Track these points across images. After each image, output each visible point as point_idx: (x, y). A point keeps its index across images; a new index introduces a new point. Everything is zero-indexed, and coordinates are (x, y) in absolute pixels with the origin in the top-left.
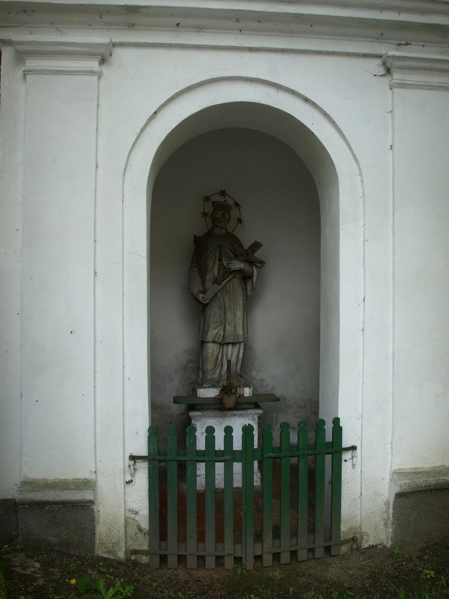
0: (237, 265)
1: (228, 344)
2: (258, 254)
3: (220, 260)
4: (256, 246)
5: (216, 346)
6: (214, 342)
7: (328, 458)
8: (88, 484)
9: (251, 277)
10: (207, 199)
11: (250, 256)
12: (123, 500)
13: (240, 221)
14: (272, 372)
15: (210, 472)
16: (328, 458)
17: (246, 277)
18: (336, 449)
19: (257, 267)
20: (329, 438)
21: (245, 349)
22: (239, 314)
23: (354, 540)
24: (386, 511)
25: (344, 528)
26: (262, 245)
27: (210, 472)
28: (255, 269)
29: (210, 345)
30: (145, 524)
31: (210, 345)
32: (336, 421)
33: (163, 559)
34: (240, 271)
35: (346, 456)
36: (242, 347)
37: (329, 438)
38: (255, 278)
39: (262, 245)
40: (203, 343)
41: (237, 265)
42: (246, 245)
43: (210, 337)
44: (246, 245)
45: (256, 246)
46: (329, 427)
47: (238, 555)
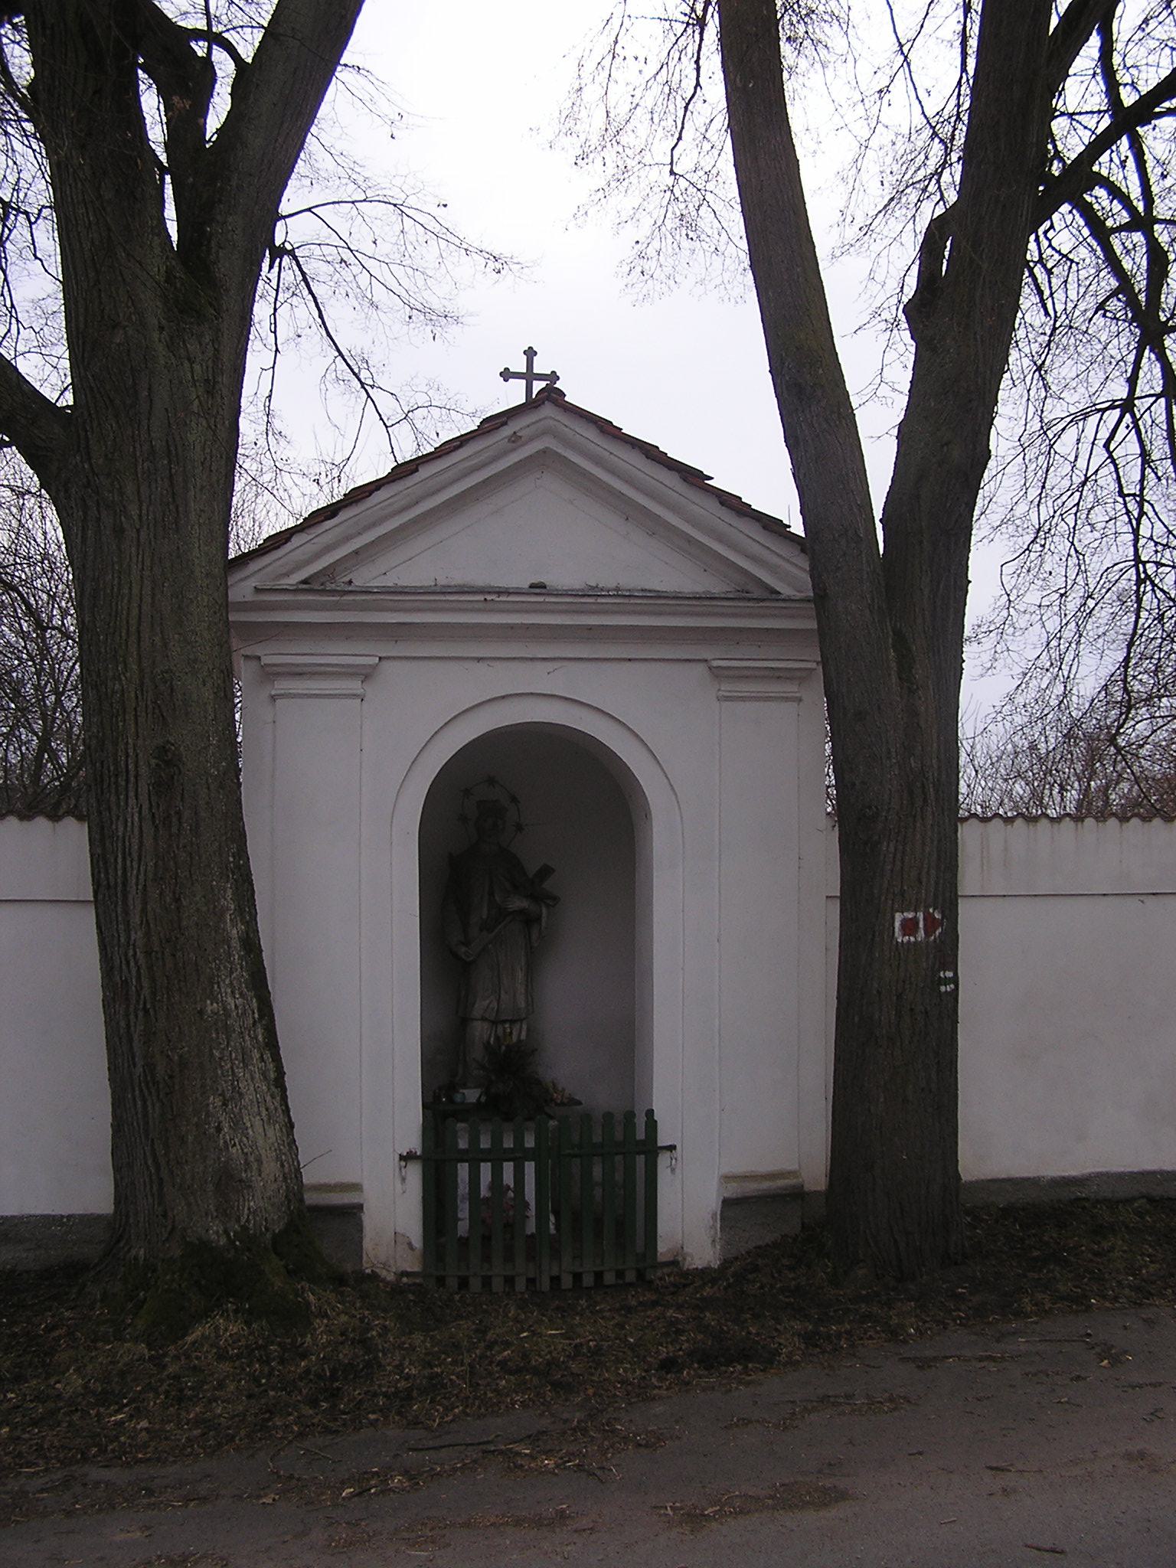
0: (518, 903)
1: (504, 1021)
2: (547, 885)
3: (491, 894)
4: (546, 872)
5: (486, 1025)
6: (483, 1019)
7: (641, 1160)
8: (356, 1187)
9: (539, 919)
10: (467, 792)
11: (538, 889)
12: (393, 1216)
13: (519, 828)
14: (568, 1065)
15: (497, 1174)
16: (641, 1160)
17: (529, 920)
18: (651, 1149)
19: (548, 906)
20: (641, 1135)
21: (528, 1030)
22: (520, 975)
23: (674, 1263)
24: (713, 1227)
25: (662, 1247)
26: (554, 870)
27: (497, 1174)
28: (544, 910)
29: (478, 1025)
30: (417, 1242)
31: (478, 1025)
32: (650, 1113)
33: (441, 1281)
34: (522, 911)
35: (663, 1160)
36: (525, 1027)
37: (641, 1135)
38: (544, 920)
39: (554, 870)
40: (464, 1022)
41: (518, 903)
42: (532, 869)
43: (477, 1012)
44: (532, 869)
45: (546, 872)
46: (641, 1122)
47: (531, 1276)
